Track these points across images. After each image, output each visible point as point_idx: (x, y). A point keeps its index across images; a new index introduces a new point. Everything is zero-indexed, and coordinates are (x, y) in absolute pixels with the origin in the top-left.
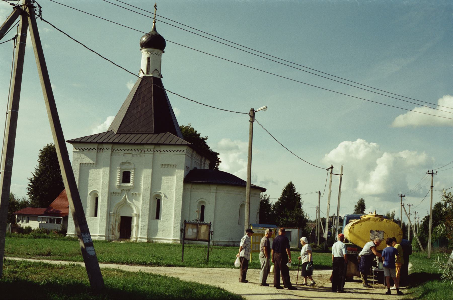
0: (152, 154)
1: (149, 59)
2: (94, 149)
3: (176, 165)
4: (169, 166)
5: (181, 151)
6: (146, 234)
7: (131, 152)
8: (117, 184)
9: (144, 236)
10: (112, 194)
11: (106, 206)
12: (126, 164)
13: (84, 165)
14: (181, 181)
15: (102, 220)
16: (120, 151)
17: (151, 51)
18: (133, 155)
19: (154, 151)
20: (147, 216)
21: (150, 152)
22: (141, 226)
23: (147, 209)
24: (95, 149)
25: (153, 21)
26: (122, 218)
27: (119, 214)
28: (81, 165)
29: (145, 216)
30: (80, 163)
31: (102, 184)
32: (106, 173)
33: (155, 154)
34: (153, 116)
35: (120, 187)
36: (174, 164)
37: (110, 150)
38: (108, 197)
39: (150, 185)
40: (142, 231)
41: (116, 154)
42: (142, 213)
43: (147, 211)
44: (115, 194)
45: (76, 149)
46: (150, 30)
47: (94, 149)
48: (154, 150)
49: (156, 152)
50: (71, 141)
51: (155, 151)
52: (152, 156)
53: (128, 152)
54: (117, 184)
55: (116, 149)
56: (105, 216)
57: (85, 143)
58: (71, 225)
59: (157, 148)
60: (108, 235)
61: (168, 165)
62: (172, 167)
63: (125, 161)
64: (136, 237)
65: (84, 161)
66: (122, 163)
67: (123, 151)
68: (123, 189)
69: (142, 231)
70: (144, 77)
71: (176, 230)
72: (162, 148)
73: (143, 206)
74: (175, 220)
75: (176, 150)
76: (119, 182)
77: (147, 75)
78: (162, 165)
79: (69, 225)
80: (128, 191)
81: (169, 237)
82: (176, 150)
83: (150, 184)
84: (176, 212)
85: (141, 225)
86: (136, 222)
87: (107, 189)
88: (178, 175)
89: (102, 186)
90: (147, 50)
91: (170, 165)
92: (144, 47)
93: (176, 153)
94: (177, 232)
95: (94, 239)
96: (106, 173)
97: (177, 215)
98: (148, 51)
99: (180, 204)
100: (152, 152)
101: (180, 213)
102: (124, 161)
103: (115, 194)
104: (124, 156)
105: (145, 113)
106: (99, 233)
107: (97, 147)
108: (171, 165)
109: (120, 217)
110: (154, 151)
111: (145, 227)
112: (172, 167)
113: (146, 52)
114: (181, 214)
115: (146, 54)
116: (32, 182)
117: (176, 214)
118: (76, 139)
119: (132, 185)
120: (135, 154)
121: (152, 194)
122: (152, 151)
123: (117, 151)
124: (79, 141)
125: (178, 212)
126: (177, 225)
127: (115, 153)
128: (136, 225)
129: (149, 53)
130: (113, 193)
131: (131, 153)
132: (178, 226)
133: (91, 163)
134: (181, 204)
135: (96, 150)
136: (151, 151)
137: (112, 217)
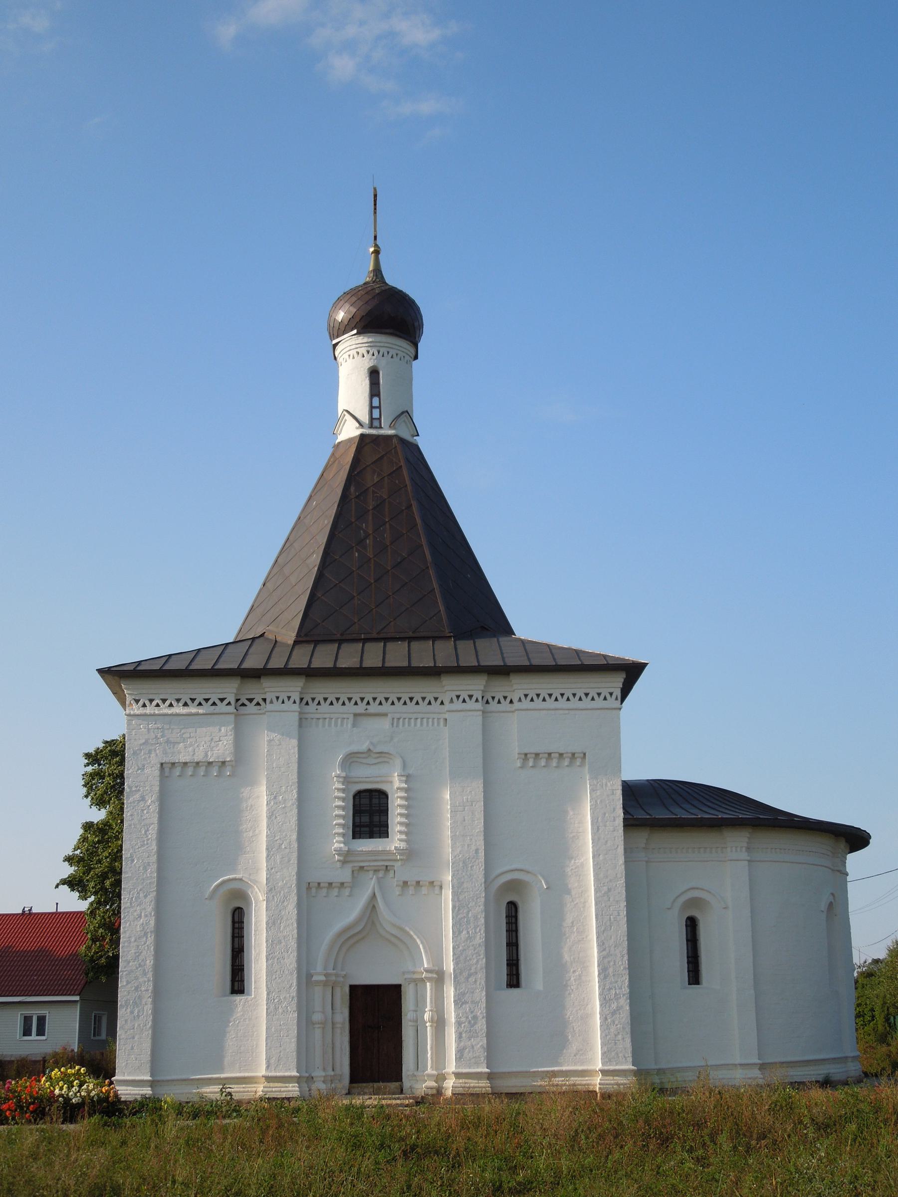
0: (481, 713)
1: (374, 374)
2: (178, 700)
3: (585, 754)
4: (554, 760)
5: (538, 695)
6: (483, 1055)
7: (386, 707)
8: (337, 844)
9: (477, 1064)
10: (314, 890)
11: (293, 944)
12: (364, 761)
13: (177, 771)
14: (614, 820)
15: (276, 1009)
16: (337, 706)
17: (382, 344)
18: (395, 720)
19: (485, 699)
20: (481, 976)
21: (471, 704)
22: (459, 1023)
23: (480, 945)
24: (226, 702)
25: (372, 250)
26: (353, 988)
27: (345, 976)
28: (167, 770)
29: (472, 979)
30: (162, 764)
31: (267, 849)
32: (285, 801)
33: (491, 712)
34: (431, 572)
35: (347, 857)
36: (571, 749)
37: (295, 702)
38: (299, 905)
39: (480, 843)
40: (462, 1044)
41: (318, 719)
42: (456, 963)
43: (478, 954)
44: (336, 890)
45: (181, 704)
46: (362, 276)
47: (222, 700)
48: (302, 699)
49: (493, 705)
50: (125, 668)
51: (307, 704)
52: (480, 719)
53: (374, 708)
54: (336, 845)
55: (320, 698)
56: (290, 987)
57: (214, 673)
58: (133, 1038)
59: (500, 687)
60: (307, 1075)
61: (550, 754)
62: (566, 762)
63: (364, 747)
64: (435, 1072)
65: (179, 752)
66: (351, 754)
67: (350, 706)
68: (362, 868)
69: (462, 1044)
70: (362, 436)
71: (613, 1029)
72: (519, 686)
73: (460, 932)
74: (605, 985)
75: (580, 693)
76: (344, 835)
77: (374, 432)
78: (526, 755)
79: (122, 1042)
80: (381, 874)
81: (582, 1064)
82: (393, 697)
83: (482, 838)
84: (605, 953)
85: (457, 1016)
86: (431, 1007)
87: (291, 872)
88: (598, 793)
89: (268, 856)
90: (366, 340)
91: (557, 755)
92: (355, 331)
93: (580, 705)
94: (620, 1037)
95: (245, 1097)
96: (285, 801)
97: (609, 962)
98: (372, 345)
99: (619, 915)
100: (479, 706)
101: (623, 956)
102: (354, 748)
103: (336, 890)
104: (354, 725)
105: (351, 573)
106: (268, 1067)
107: (299, 689)
108: (561, 755)
109: (347, 990)
110: (304, 701)
111: (476, 1027)
112: (566, 762)
113: (363, 350)
114: (626, 958)
115: (363, 356)
116: (30, 910)
117: (606, 961)
118: (140, 663)
119: (403, 845)
120: (405, 716)
121: (493, 880)
122: (477, 700)
123: (325, 707)
124: (212, 668)
125: (612, 949)
126: (614, 1006)
127: (318, 716)
128: (432, 1021)
129: (376, 353)
130: (319, 884)
131: (385, 715)
132: (619, 1008)
133: (210, 763)
134: (624, 913)
135: (229, 704)
136: (474, 699)
137: (318, 991)
